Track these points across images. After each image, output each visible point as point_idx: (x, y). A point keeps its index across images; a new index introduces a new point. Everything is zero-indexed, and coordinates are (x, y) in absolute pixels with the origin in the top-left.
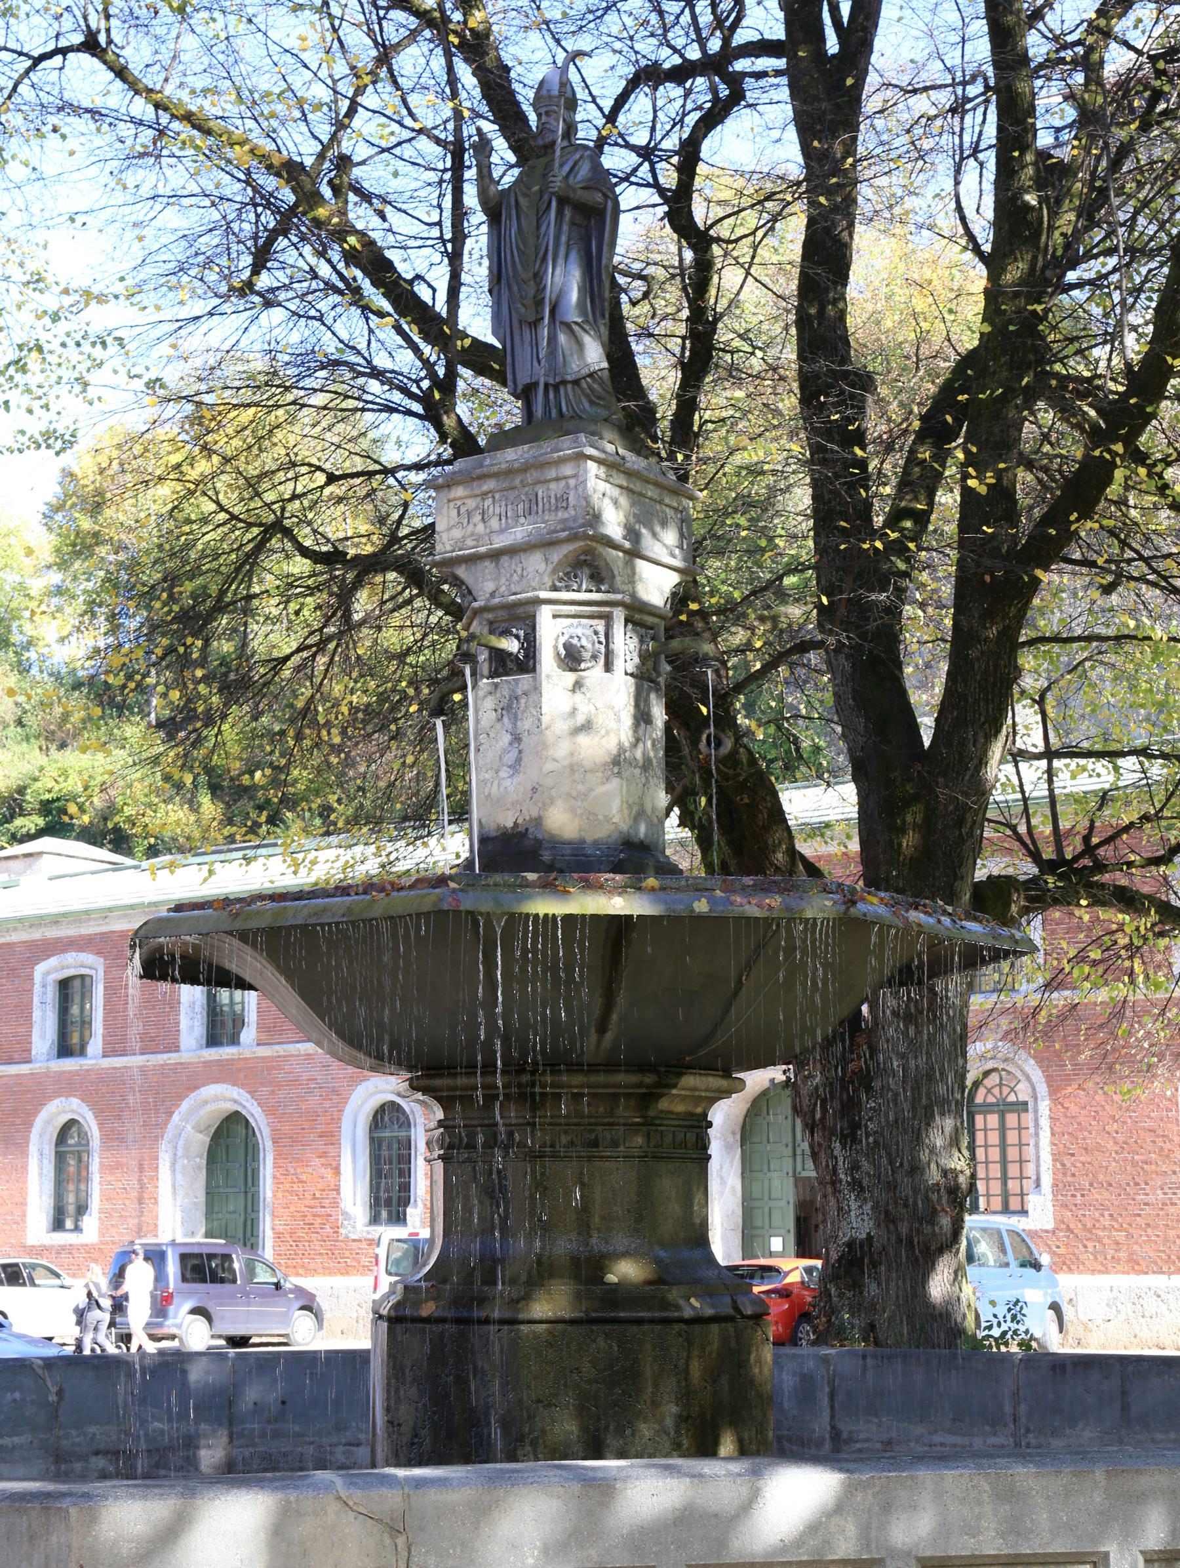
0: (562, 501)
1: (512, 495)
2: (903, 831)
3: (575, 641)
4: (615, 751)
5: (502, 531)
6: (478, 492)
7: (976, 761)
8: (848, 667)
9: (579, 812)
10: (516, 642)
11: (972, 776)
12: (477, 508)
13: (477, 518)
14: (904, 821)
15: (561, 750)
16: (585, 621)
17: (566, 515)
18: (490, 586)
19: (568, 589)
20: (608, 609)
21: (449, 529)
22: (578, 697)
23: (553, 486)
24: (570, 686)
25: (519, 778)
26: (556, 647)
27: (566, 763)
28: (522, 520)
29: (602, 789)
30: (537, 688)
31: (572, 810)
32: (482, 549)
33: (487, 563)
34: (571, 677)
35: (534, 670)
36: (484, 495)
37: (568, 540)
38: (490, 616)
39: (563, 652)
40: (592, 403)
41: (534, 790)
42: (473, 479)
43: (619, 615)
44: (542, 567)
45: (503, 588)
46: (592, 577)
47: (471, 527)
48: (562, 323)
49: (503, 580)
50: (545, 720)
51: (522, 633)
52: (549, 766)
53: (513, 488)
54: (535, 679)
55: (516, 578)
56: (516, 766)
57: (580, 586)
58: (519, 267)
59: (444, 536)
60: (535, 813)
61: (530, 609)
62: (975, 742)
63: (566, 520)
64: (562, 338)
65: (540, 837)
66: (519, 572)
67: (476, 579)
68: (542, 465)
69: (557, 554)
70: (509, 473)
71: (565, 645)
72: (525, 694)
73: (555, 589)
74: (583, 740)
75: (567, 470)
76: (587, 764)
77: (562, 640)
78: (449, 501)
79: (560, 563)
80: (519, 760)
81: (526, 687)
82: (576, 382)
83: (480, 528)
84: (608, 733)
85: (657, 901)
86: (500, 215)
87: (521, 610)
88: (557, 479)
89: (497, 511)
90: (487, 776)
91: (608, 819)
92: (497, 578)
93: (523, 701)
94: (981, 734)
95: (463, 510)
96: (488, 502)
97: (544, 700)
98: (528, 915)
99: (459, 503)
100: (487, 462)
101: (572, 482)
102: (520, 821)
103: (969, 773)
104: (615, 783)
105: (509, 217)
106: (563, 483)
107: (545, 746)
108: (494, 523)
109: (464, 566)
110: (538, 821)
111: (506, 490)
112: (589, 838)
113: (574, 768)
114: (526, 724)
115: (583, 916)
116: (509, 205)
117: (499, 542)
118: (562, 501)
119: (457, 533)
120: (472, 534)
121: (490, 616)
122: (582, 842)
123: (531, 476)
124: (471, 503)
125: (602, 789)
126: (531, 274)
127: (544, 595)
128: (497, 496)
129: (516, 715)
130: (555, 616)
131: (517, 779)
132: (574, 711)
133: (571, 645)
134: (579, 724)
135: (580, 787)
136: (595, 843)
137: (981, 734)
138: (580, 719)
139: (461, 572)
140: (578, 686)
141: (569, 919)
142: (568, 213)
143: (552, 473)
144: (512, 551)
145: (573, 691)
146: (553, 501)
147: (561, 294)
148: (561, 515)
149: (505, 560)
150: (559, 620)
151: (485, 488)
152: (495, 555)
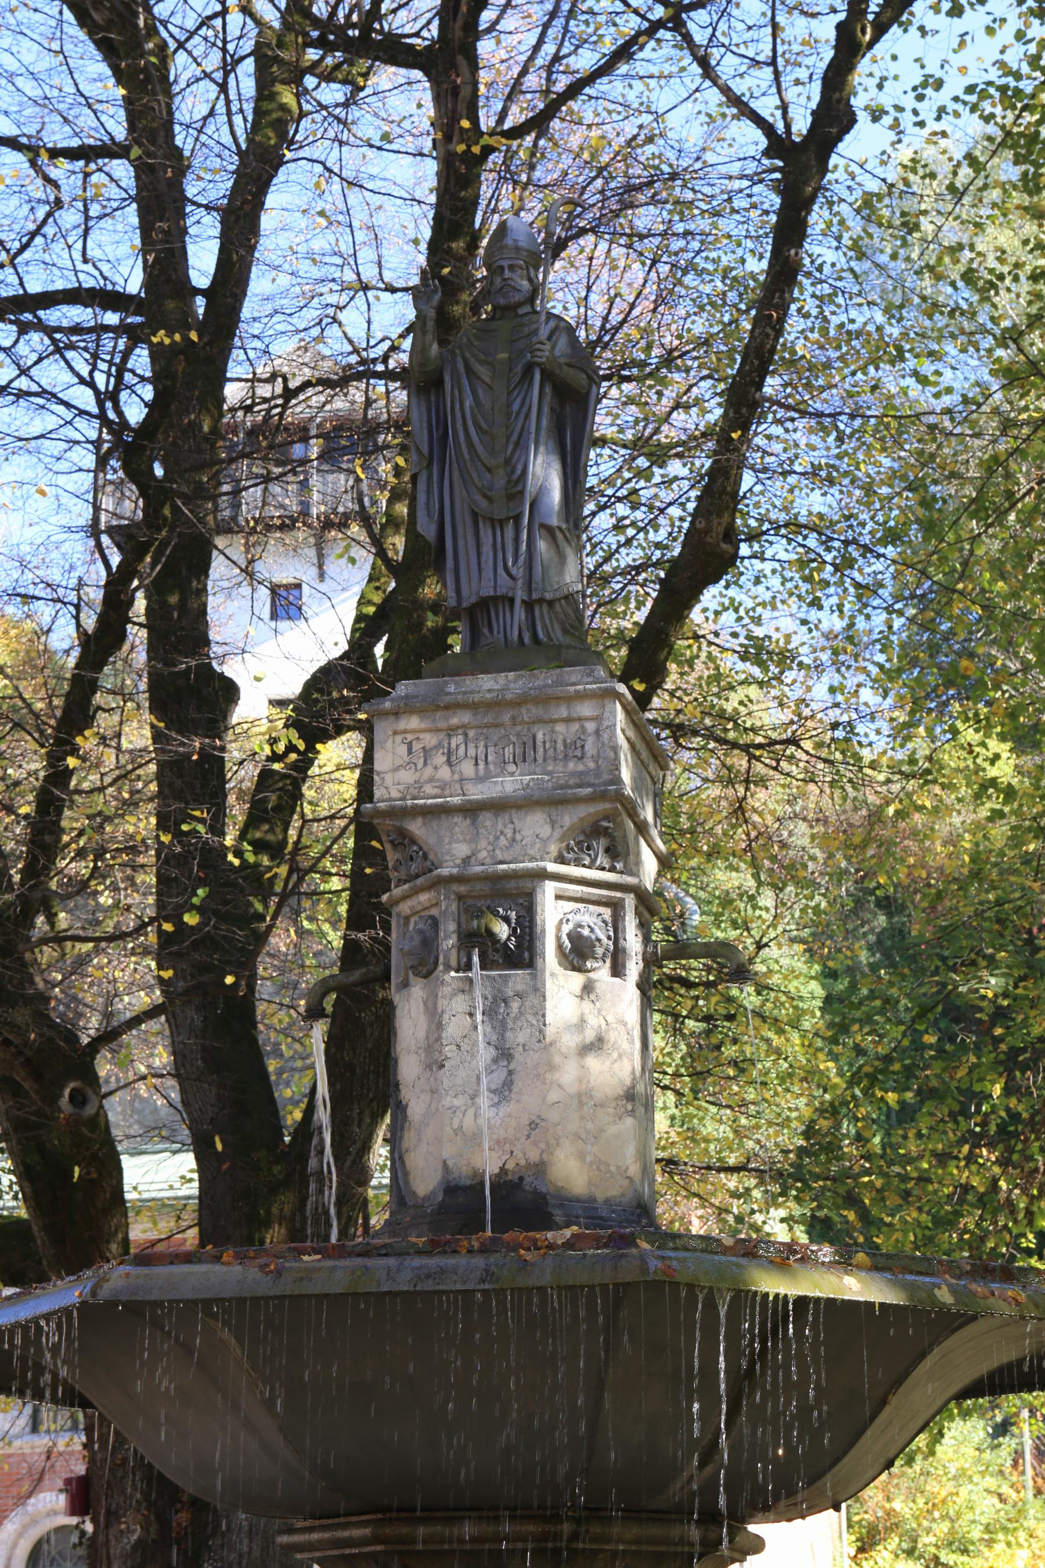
0: (574, 749)
1: (495, 735)
2: (267, 1224)
3: (586, 932)
4: (628, 1082)
5: (479, 779)
6: (443, 725)
7: (359, 1145)
8: (198, 1019)
9: (588, 1159)
10: (505, 927)
11: (353, 1162)
12: (439, 746)
13: (440, 759)
14: (268, 1212)
15: (568, 1074)
16: (591, 907)
17: (581, 767)
18: (462, 850)
19: (578, 862)
20: (619, 895)
21: (396, 769)
22: (587, 1006)
23: (560, 728)
24: (578, 992)
25: (510, 1108)
26: (558, 938)
27: (573, 1090)
28: (512, 768)
29: (612, 1130)
30: (538, 991)
31: (581, 1156)
32: (456, 800)
33: (458, 819)
34: (577, 980)
35: (530, 964)
36: (451, 731)
37: (590, 799)
38: (463, 889)
39: (567, 944)
40: (565, 631)
41: (533, 1125)
42: (438, 708)
43: (630, 901)
44: (546, 831)
45: (483, 854)
46: (607, 850)
47: (428, 771)
48: (543, 526)
49: (483, 844)
50: (550, 1031)
51: (513, 915)
52: (553, 1096)
53: (496, 726)
54: (534, 977)
55: (503, 841)
56: (503, 1092)
57: (593, 861)
58: (480, 449)
59: (389, 778)
60: (534, 1156)
61: (528, 884)
62: (360, 1121)
63: (581, 773)
64: (542, 545)
65: (544, 1190)
66: (509, 835)
67: (440, 839)
68: (544, 699)
69: (569, 818)
70: (496, 704)
71: (569, 935)
72: (518, 995)
73: (561, 860)
74: (593, 1062)
75: (586, 709)
76: (599, 1096)
77: (566, 929)
78: (395, 733)
79: (571, 829)
80: (508, 1084)
81: (519, 987)
82: (550, 603)
83: (445, 773)
84: (620, 1056)
85: (895, 1283)
86: (439, 383)
87: (512, 884)
88: (568, 720)
89: (472, 752)
90: (457, 1102)
91: (622, 1171)
92: (474, 840)
93: (515, 1005)
94: (367, 1113)
95: (416, 747)
96: (457, 740)
97: (549, 1005)
98: (756, 1293)
99: (410, 737)
100: (452, 688)
101: (591, 726)
102: (510, 1166)
103: (350, 1159)
104: (629, 1121)
105: (457, 384)
106: (576, 726)
107: (552, 1067)
108: (467, 769)
109: (419, 820)
110: (540, 1168)
111: (487, 726)
112: (600, 1197)
113: (583, 1098)
114: (519, 1036)
115: (818, 1300)
116: (455, 372)
117: (477, 793)
118: (574, 749)
119: (407, 776)
120: (431, 780)
121: (463, 889)
122: (592, 1200)
123: (527, 713)
124: (430, 740)
125: (612, 1130)
126: (501, 459)
127: (552, 867)
128: (471, 733)
129: (503, 1024)
130: (558, 897)
131: (504, 1110)
132: (582, 1023)
133: (580, 936)
134: (588, 1041)
135: (590, 1126)
136: (607, 1201)
137: (367, 1113)
138: (590, 1035)
139: (415, 827)
140: (588, 988)
141: (802, 1302)
142: (548, 390)
143: (563, 712)
144: (499, 806)
145: (581, 998)
146: (560, 746)
147: (542, 491)
148: (571, 765)
149: (486, 819)
150: (561, 903)
151: (455, 721)
152: (472, 810)
